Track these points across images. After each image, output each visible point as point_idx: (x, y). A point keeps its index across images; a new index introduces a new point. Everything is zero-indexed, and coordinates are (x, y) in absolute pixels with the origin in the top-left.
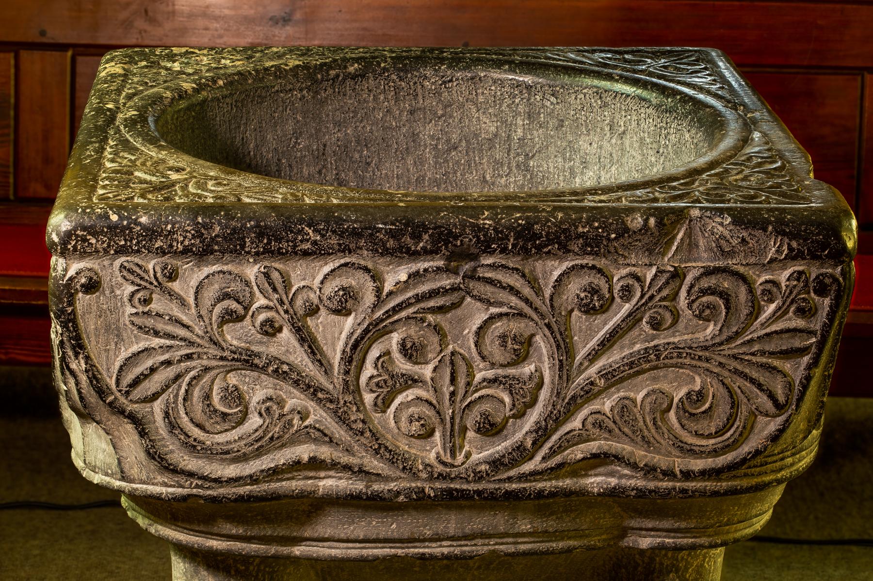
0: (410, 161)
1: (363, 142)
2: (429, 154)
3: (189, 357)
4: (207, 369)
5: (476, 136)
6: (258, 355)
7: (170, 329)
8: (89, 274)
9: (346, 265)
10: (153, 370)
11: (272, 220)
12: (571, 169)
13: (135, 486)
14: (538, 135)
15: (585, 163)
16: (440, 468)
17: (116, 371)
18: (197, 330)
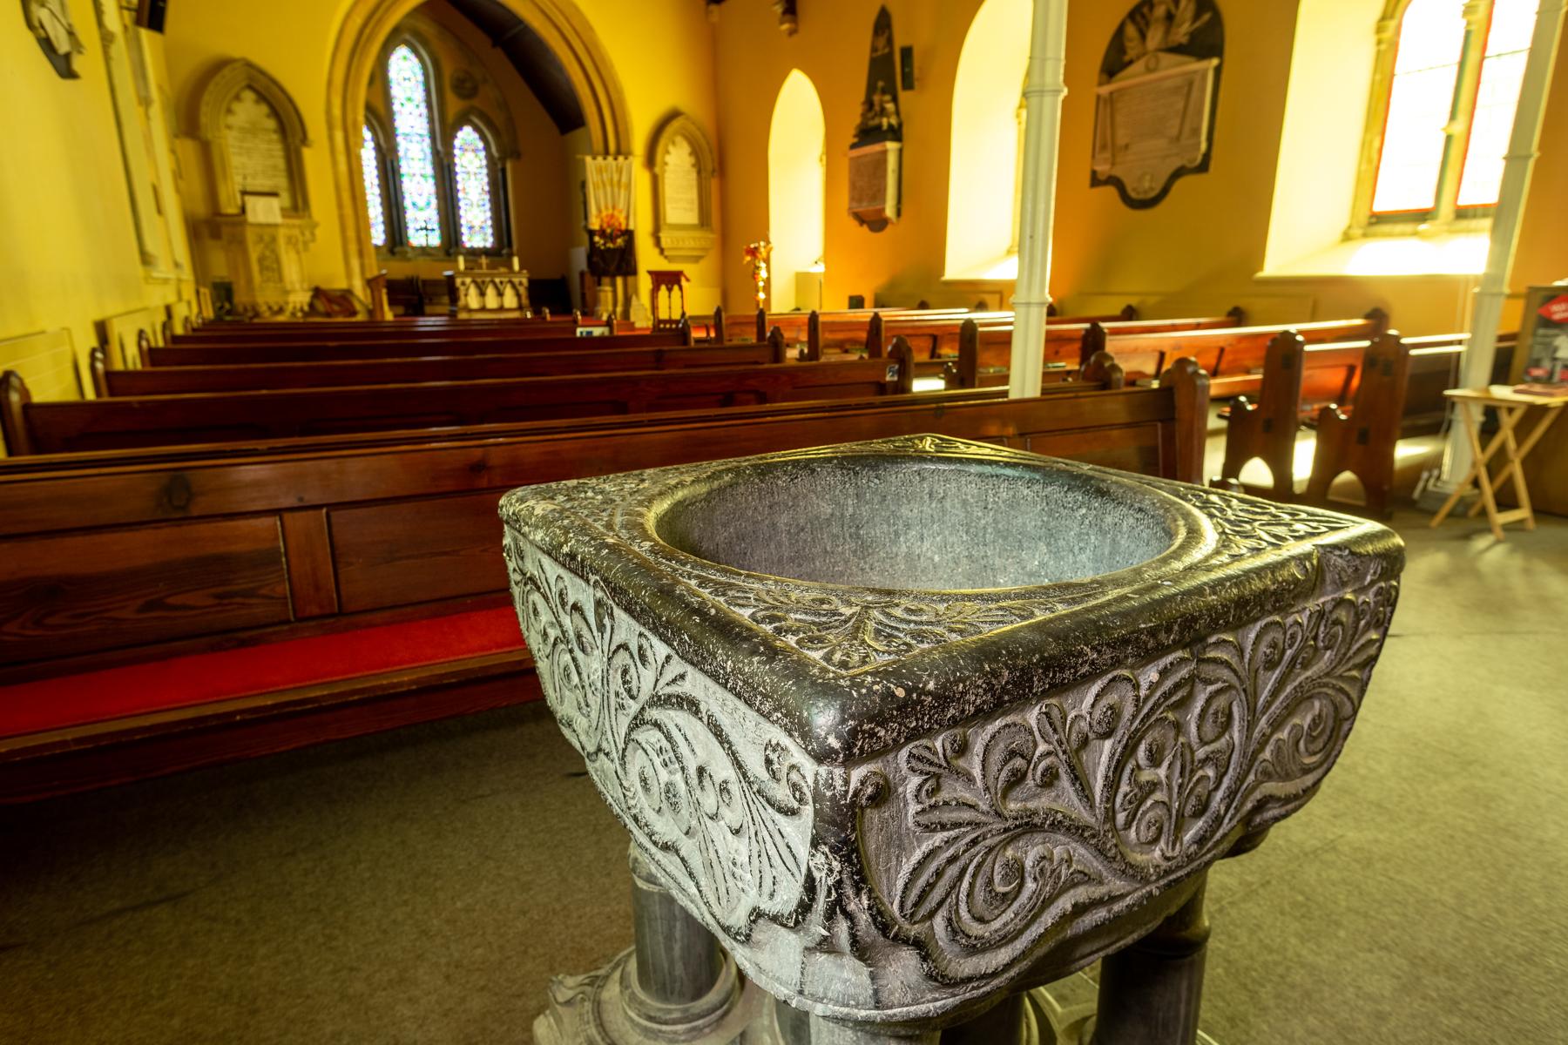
0: (772, 546)
1: (741, 537)
2: (784, 538)
3: (974, 842)
4: (991, 849)
5: (817, 518)
6: (1035, 813)
7: (956, 816)
8: (874, 779)
9: (1111, 681)
10: (939, 874)
11: (1053, 649)
12: (896, 533)
13: (889, 1012)
14: (865, 511)
15: (908, 526)
16: (1165, 865)
17: (899, 893)
18: (984, 807)
